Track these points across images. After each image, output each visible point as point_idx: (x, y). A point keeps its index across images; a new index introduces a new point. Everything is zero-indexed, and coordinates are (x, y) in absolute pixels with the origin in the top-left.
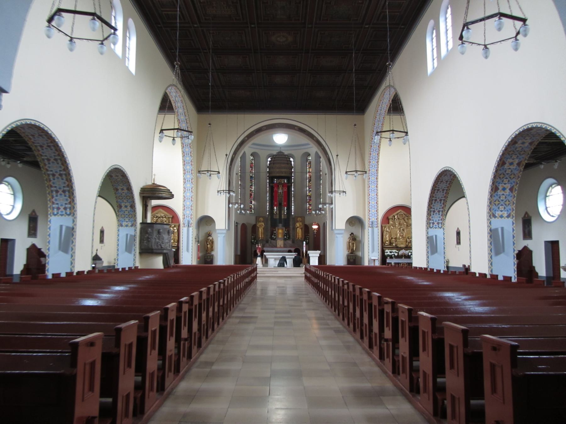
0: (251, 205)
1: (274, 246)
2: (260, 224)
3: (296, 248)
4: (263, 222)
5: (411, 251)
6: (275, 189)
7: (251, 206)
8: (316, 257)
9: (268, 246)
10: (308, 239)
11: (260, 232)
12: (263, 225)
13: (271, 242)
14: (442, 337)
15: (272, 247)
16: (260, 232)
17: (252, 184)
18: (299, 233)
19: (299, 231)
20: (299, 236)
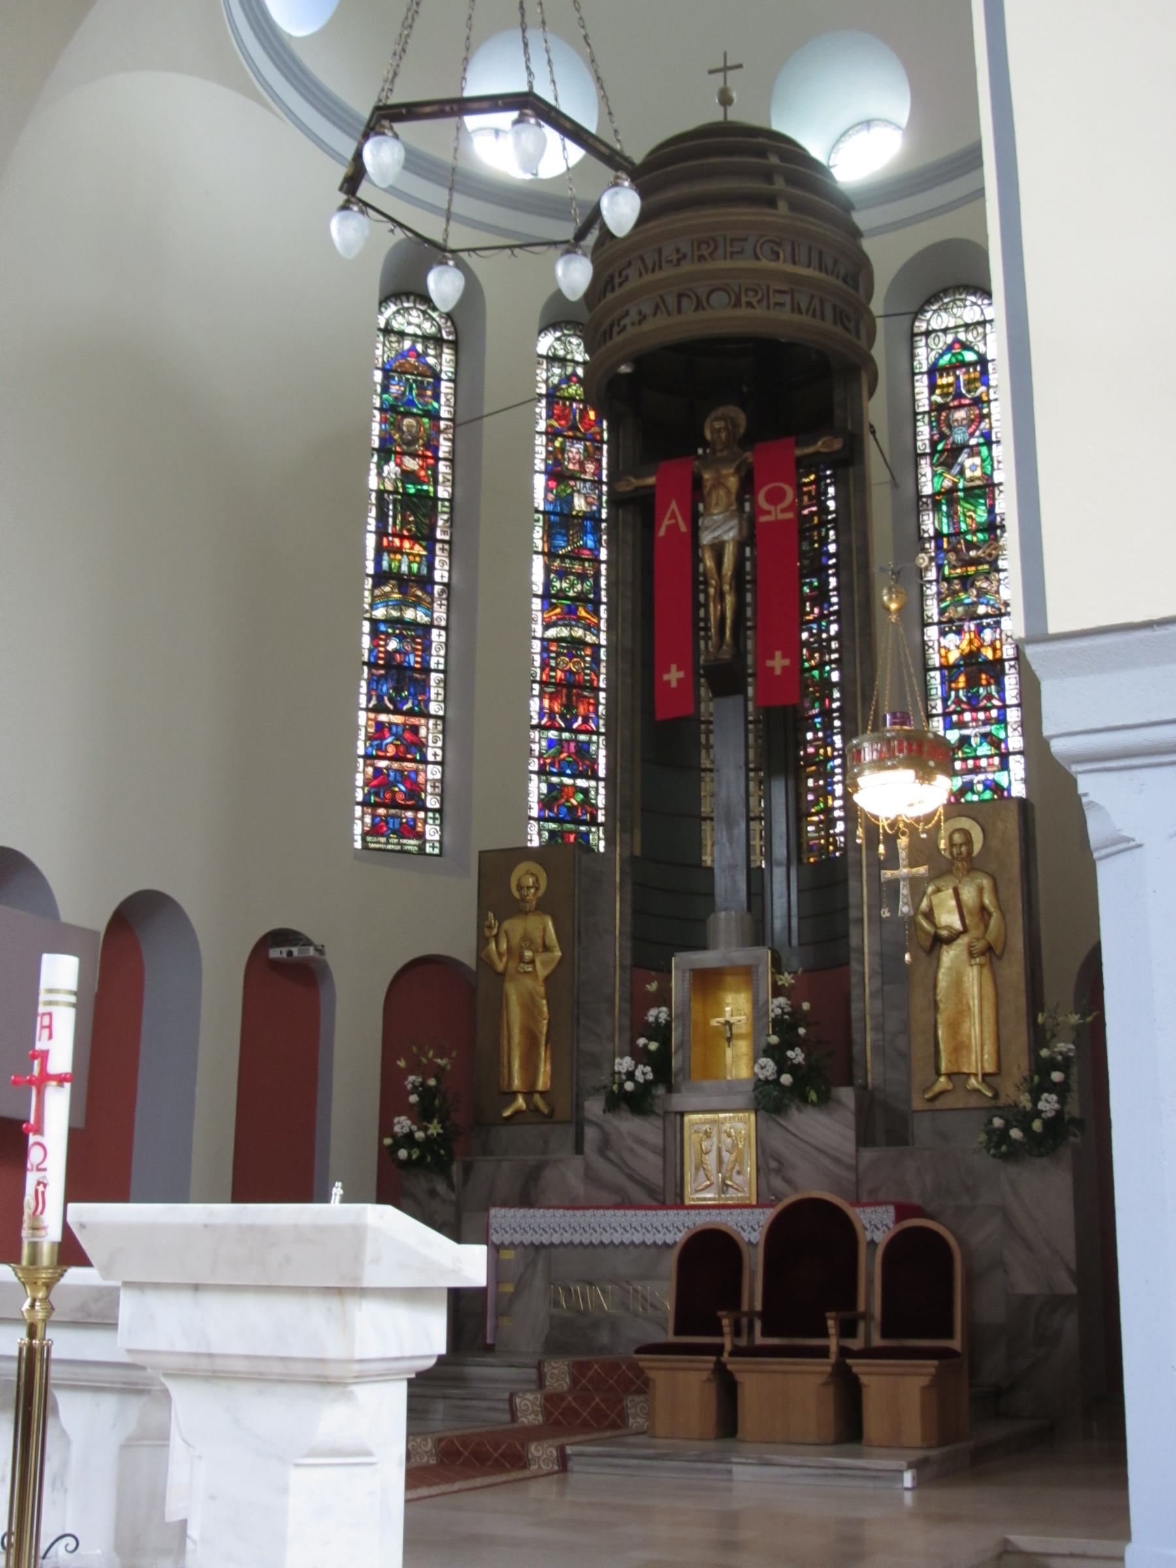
0: (582, 783)
1: (650, 1191)
2: (516, 927)
3: (786, 1202)
4: (542, 907)
5: (554, 1311)
6: (666, 522)
7: (585, 791)
8: (706, 1370)
9: (578, 1186)
10: (1057, 1076)
11: (517, 1037)
12: (546, 948)
13: (604, 1146)
14: (639, 181)
15: (625, 1203)
16: (517, 1037)
17: (596, 587)
18: (962, 1012)
19: (958, 983)
20: (959, 1048)
